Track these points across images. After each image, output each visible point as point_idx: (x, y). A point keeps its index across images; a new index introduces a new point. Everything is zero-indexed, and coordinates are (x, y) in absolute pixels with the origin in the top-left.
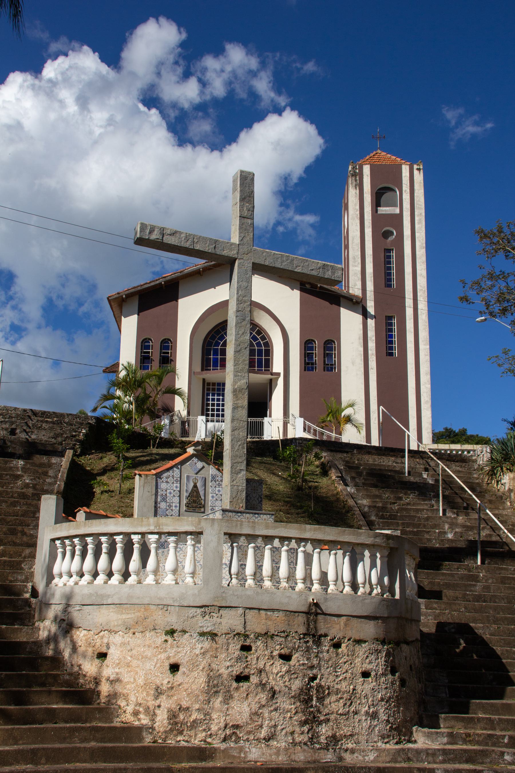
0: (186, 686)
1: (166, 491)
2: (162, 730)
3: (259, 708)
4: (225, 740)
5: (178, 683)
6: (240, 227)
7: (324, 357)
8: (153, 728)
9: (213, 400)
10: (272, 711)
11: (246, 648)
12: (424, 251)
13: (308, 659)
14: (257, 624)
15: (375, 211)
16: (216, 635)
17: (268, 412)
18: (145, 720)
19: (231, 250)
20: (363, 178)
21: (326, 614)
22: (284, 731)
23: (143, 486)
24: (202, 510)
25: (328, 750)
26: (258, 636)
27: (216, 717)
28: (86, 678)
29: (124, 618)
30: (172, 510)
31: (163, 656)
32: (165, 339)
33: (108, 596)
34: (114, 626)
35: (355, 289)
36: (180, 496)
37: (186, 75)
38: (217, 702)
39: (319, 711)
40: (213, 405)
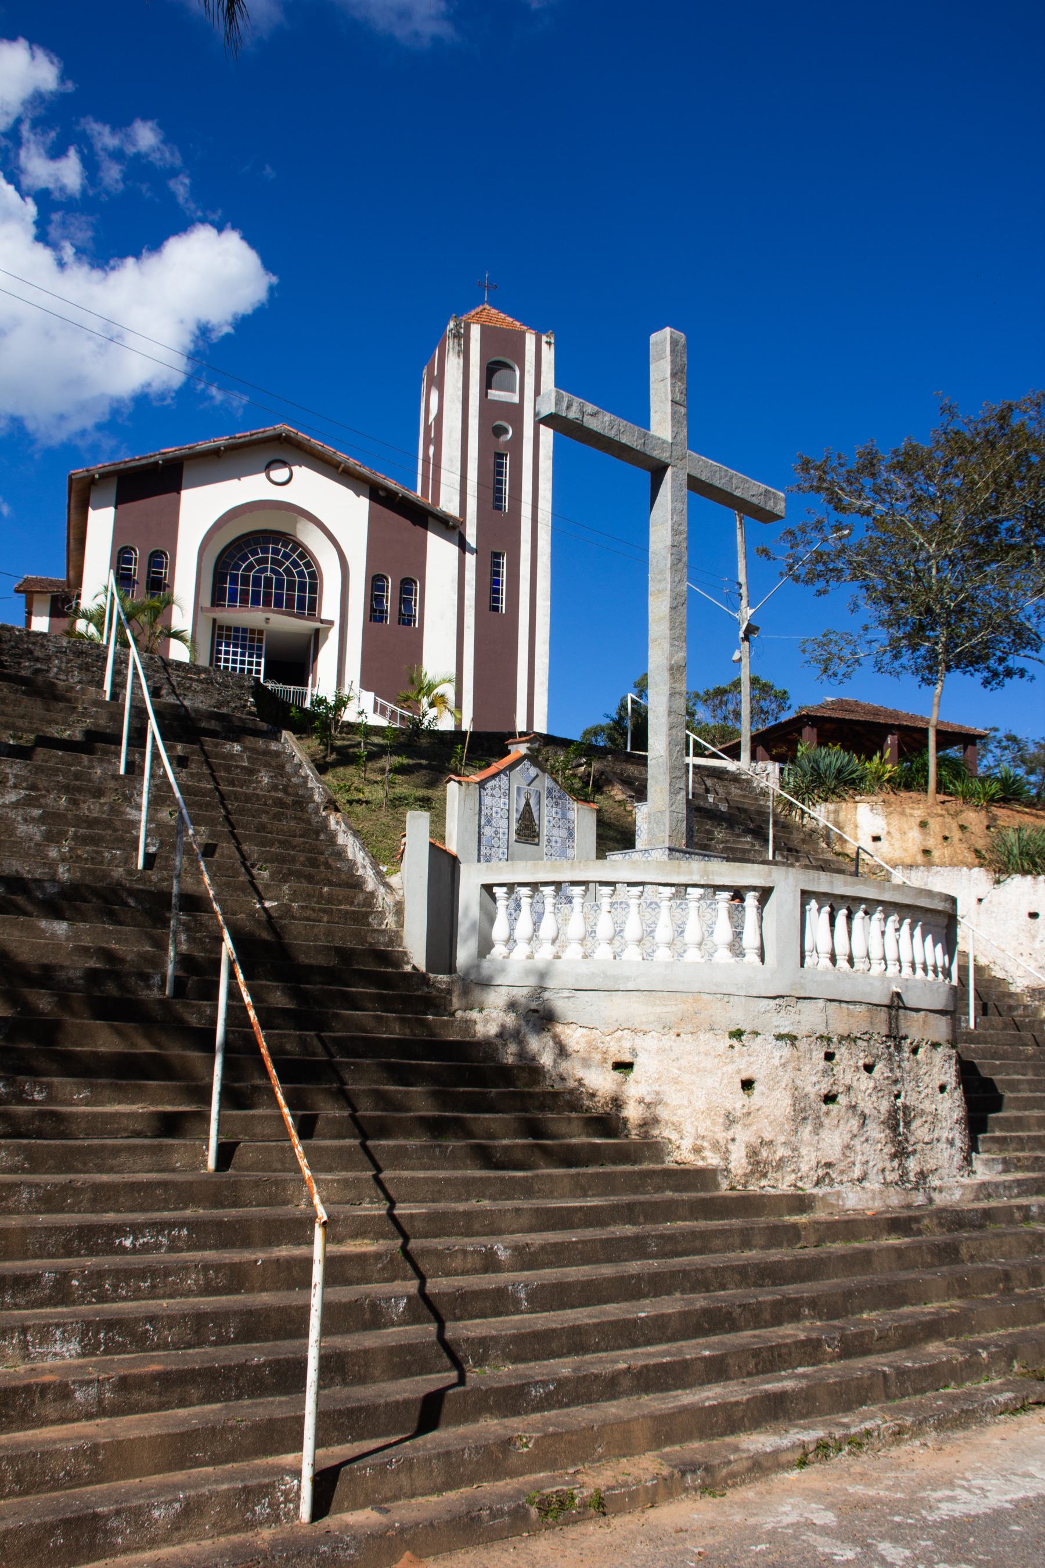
0: (766, 1111)
2: (740, 1172)
3: (851, 1139)
4: (817, 1184)
8: (728, 1171)
9: (227, 653)
11: (829, 1057)
12: (550, 463)
13: (891, 1070)
14: (840, 1023)
16: (795, 1038)
17: (310, 678)
18: (713, 1160)
19: (663, 450)
21: (906, 1008)
22: (875, 1168)
23: (463, 800)
24: (537, 840)
25: (918, 1190)
26: (842, 1038)
28: (596, 1099)
31: (730, 1068)
32: (157, 551)
33: (628, 979)
35: (449, 504)
36: (508, 818)
37: (56, 153)
39: (907, 1141)
40: (234, 661)
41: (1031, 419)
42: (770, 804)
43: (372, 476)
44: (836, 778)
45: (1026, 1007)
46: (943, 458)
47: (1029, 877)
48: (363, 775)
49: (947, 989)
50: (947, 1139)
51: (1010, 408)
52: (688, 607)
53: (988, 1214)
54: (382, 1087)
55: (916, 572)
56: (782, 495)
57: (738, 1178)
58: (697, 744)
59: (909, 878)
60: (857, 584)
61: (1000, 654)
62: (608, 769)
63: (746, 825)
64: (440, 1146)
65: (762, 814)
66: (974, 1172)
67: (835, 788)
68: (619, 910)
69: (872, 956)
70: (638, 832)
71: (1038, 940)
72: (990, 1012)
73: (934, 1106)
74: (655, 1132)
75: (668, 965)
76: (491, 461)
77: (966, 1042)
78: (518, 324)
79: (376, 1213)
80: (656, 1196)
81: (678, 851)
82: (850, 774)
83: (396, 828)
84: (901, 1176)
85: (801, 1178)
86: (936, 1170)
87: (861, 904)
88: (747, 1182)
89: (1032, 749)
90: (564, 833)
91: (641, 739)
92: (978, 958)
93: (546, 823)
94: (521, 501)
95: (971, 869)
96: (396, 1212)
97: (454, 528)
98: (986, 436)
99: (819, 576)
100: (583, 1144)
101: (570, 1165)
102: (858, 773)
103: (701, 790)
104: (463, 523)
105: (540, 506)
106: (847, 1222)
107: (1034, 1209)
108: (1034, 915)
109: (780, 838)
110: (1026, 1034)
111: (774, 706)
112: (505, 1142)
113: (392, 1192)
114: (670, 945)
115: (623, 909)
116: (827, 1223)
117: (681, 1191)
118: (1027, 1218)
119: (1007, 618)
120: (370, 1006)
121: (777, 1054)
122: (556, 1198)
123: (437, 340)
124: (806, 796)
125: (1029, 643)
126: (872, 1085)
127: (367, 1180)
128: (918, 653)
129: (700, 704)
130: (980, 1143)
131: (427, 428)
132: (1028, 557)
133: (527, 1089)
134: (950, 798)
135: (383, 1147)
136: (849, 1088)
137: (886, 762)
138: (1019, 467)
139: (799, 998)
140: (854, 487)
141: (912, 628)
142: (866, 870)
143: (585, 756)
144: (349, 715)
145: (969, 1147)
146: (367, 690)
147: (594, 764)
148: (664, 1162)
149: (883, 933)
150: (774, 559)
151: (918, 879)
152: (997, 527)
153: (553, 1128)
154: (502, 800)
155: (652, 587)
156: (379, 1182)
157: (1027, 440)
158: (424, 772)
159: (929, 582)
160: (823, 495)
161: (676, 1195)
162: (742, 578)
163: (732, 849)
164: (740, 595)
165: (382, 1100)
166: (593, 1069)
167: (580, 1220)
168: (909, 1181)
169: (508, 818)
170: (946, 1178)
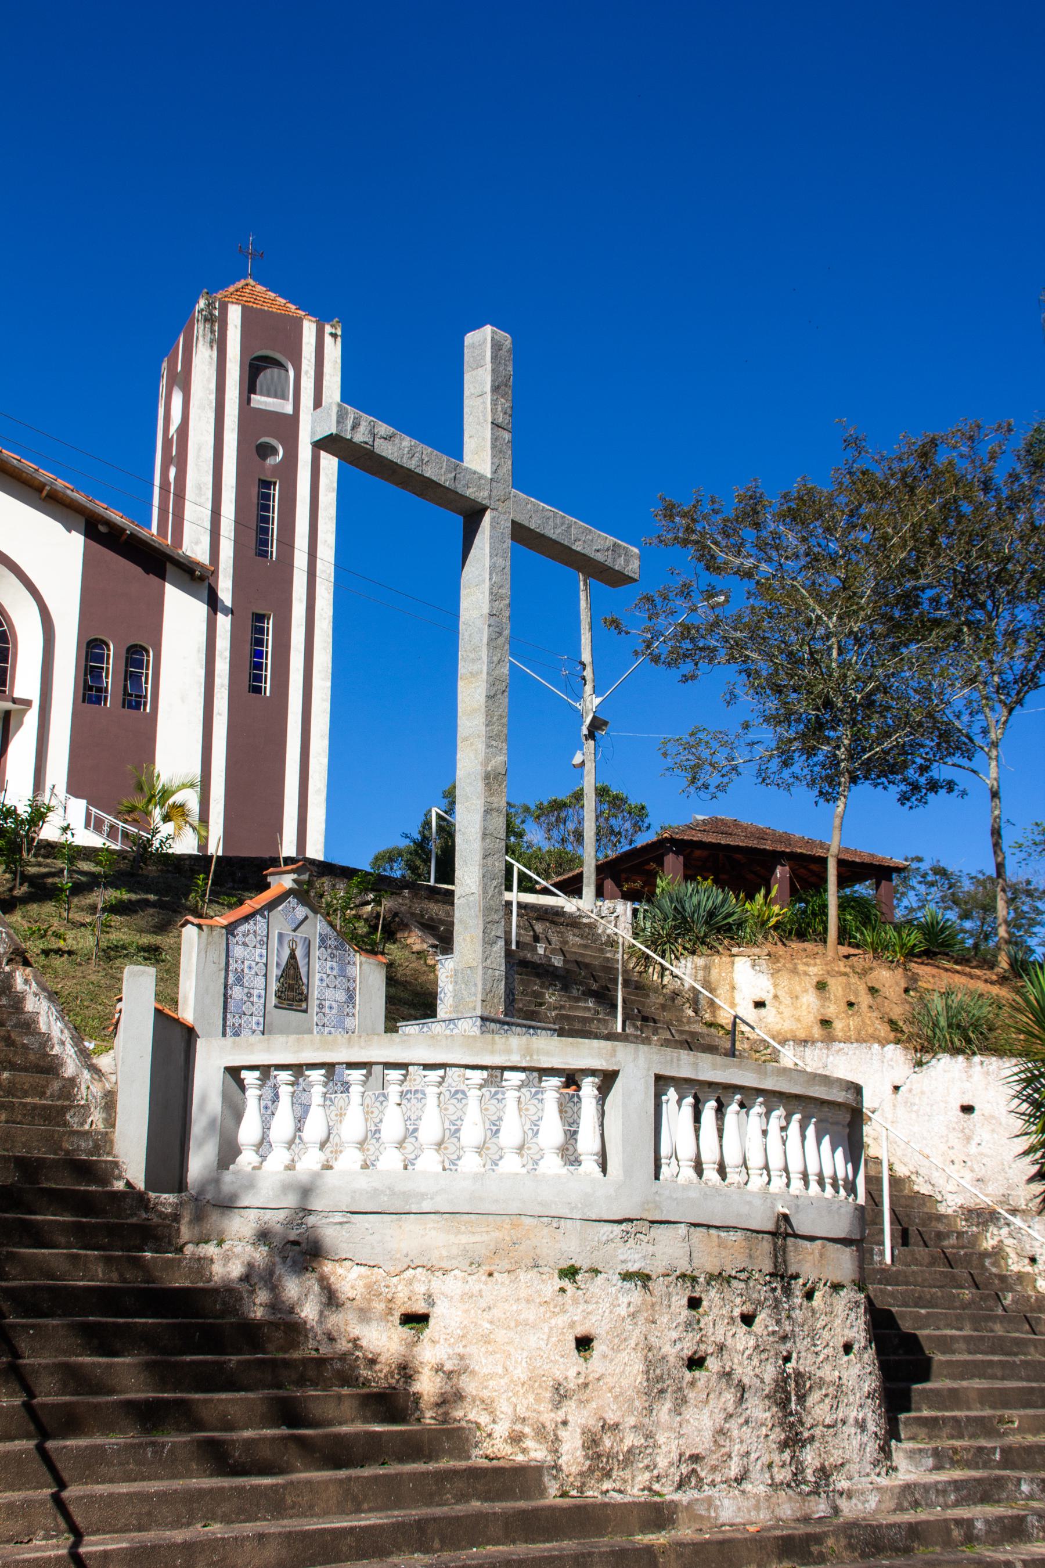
0: (610, 1381)
1: (243, 962)
2: (574, 1470)
3: (726, 1420)
4: (680, 1487)
5: (597, 1376)
6: (492, 444)
7: (126, 680)
8: (557, 1467)
10: (742, 1425)
11: (694, 1303)
12: (333, 496)
13: (778, 1322)
14: (708, 1257)
15: (245, 402)
16: (648, 1277)
18: (537, 1453)
19: (480, 488)
20: (226, 330)
22: (759, 1463)
23: (204, 951)
24: (304, 1005)
25: (819, 1494)
26: (711, 1278)
27: (665, 1440)
28: (378, 1367)
29: (463, 1241)
30: (252, 1003)
31: (561, 1321)
33: (423, 1196)
34: (441, 1258)
35: (195, 546)
36: (266, 975)
38: (664, 1409)
39: (802, 1424)
41: (962, 456)
42: (619, 956)
43: (89, 505)
44: (707, 923)
45: (960, 1234)
46: (847, 505)
47: (961, 1058)
48: (65, 914)
49: (850, 1209)
50: (856, 1420)
51: (933, 442)
52: (510, 698)
53: (914, 1531)
54: (73, 1359)
55: (811, 654)
56: (636, 550)
57: (571, 1479)
58: (522, 876)
59: (802, 1058)
60: (734, 667)
61: (922, 761)
62: (403, 909)
63: (587, 985)
64: (153, 1444)
65: (609, 969)
66: (895, 1469)
67: (705, 936)
68: (414, 1101)
69: (750, 1164)
70: (441, 996)
71: (974, 1143)
72: (912, 1240)
73: (837, 1373)
74: (458, 1414)
75: (477, 1177)
76: (254, 491)
77: (880, 1283)
78: (293, 307)
79: (52, 1553)
80: (458, 1507)
81: (493, 1021)
82: (725, 918)
83: (109, 988)
84: (795, 1474)
85: (658, 1478)
86: (842, 1465)
87: (735, 1094)
88: (583, 1484)
89: (967, 886)
90: (341, 996)
91: (447, 871)
92: (895, 1167)
93: (317, 983)
94: (292, 566)
95: (883, 1046)
96: (82, 1550)
97: (202, 579)
98: (903, 478)
99: (685, 656)
100: (357, 1434)
101: (338, 1466)
102: (735, 917)
103: (528, 939)
104: (215, 573)
105: (319, 554)
106: (722, 1543)
107: (979, 1525)
108: (968, 1109)
109: (633, 1002)
110: (960, 1272)
111: (628, 825)
112: (248, 1434)
113: (78, 1519)
114: (480, 1150)
115: (420, 1100)
116: (694, 1544)
117: (492, 1500)
118: (970, 1538)
119: (930, 715)
120: (62, 1240)
121: (624, 1300)
122: (317, 1515)
123: (183, 322)
124: (667, 946)
125: (958, 748)
126: (752, 1343)
127: (42, 1503)
128: (815, 759)
129: (530, 821)
130: (901, 1427)
131: (167, 442)
132: (957, 636)
133: (281, 1355)
134: (856, 951)
135: (71, 1449)
136: (721, 1348)
137: (774, 902)
138: (946, 519)
139: (652, 1222)
140: (732, 540)
141: (806, 726)
142: (746, 1046)
143: (372, 890)
144: (49, 832)
145: (886, 1431)
146: (77, 796)
147: (384, 902)
148: (469, 1458)
149: (765, 1133)
150: (627, 633)
151: (815, 1060)
152: (918, 596)
153: (317, 1411)
154: (258, 951)
155: (463, 668)
156: (60, 1504)
157: (957, 484)
158: (151, 911)
159: (828, 667)
160: (692, 549)
161: (486, 1507)
162: (586, 656)
163: (568, 1018)
164: (584, 678)
165: (75, 1379)
166: (374, 1324)
167: (351, 1547)
168: (806, 1482)
169: (266, 975)
170: (856, 1476)
